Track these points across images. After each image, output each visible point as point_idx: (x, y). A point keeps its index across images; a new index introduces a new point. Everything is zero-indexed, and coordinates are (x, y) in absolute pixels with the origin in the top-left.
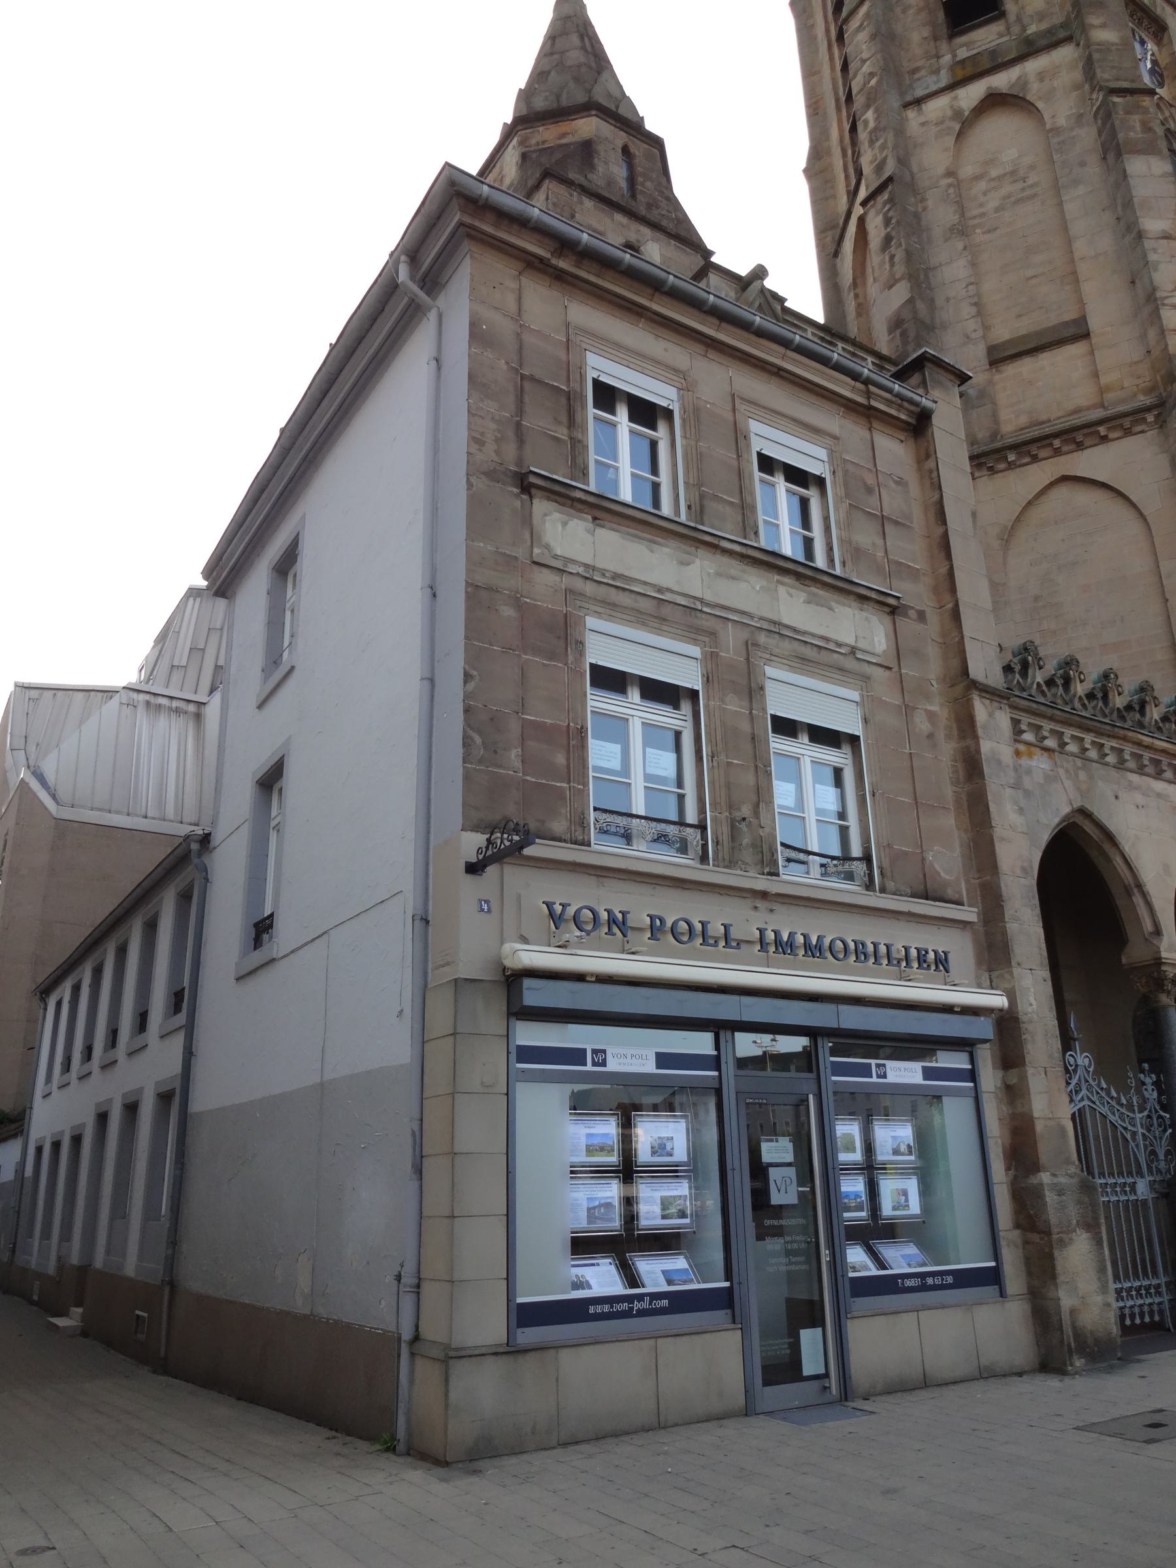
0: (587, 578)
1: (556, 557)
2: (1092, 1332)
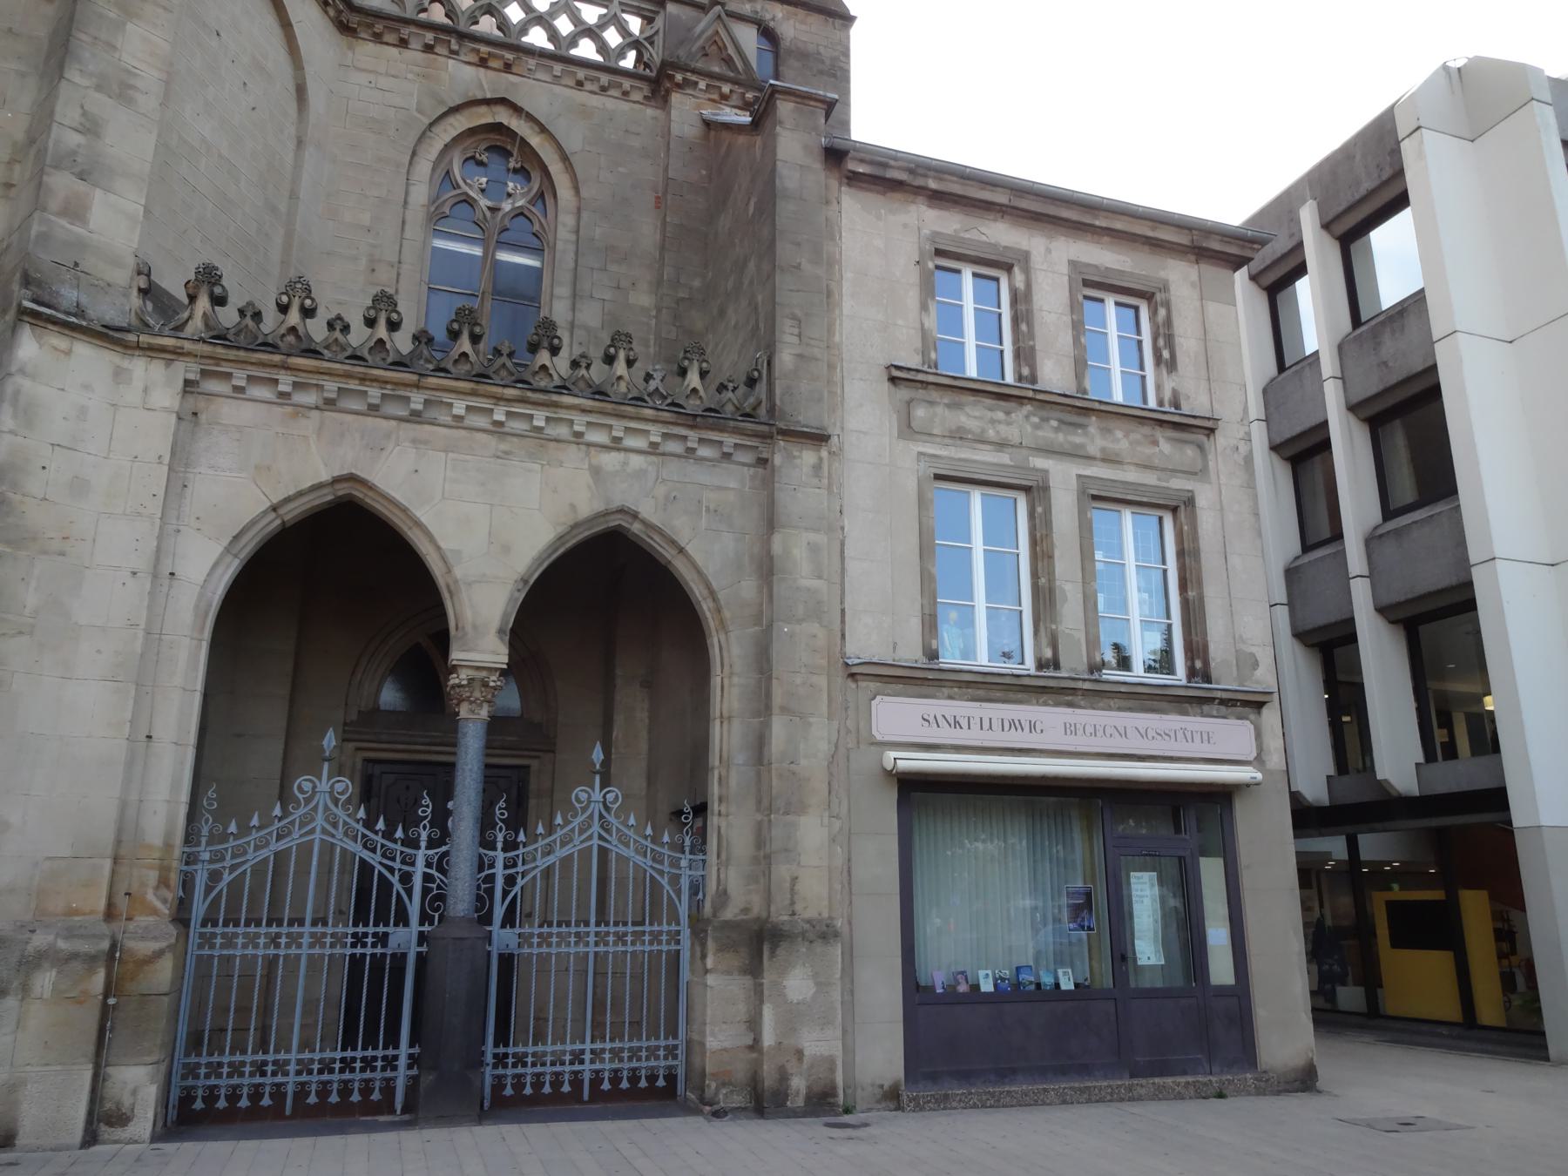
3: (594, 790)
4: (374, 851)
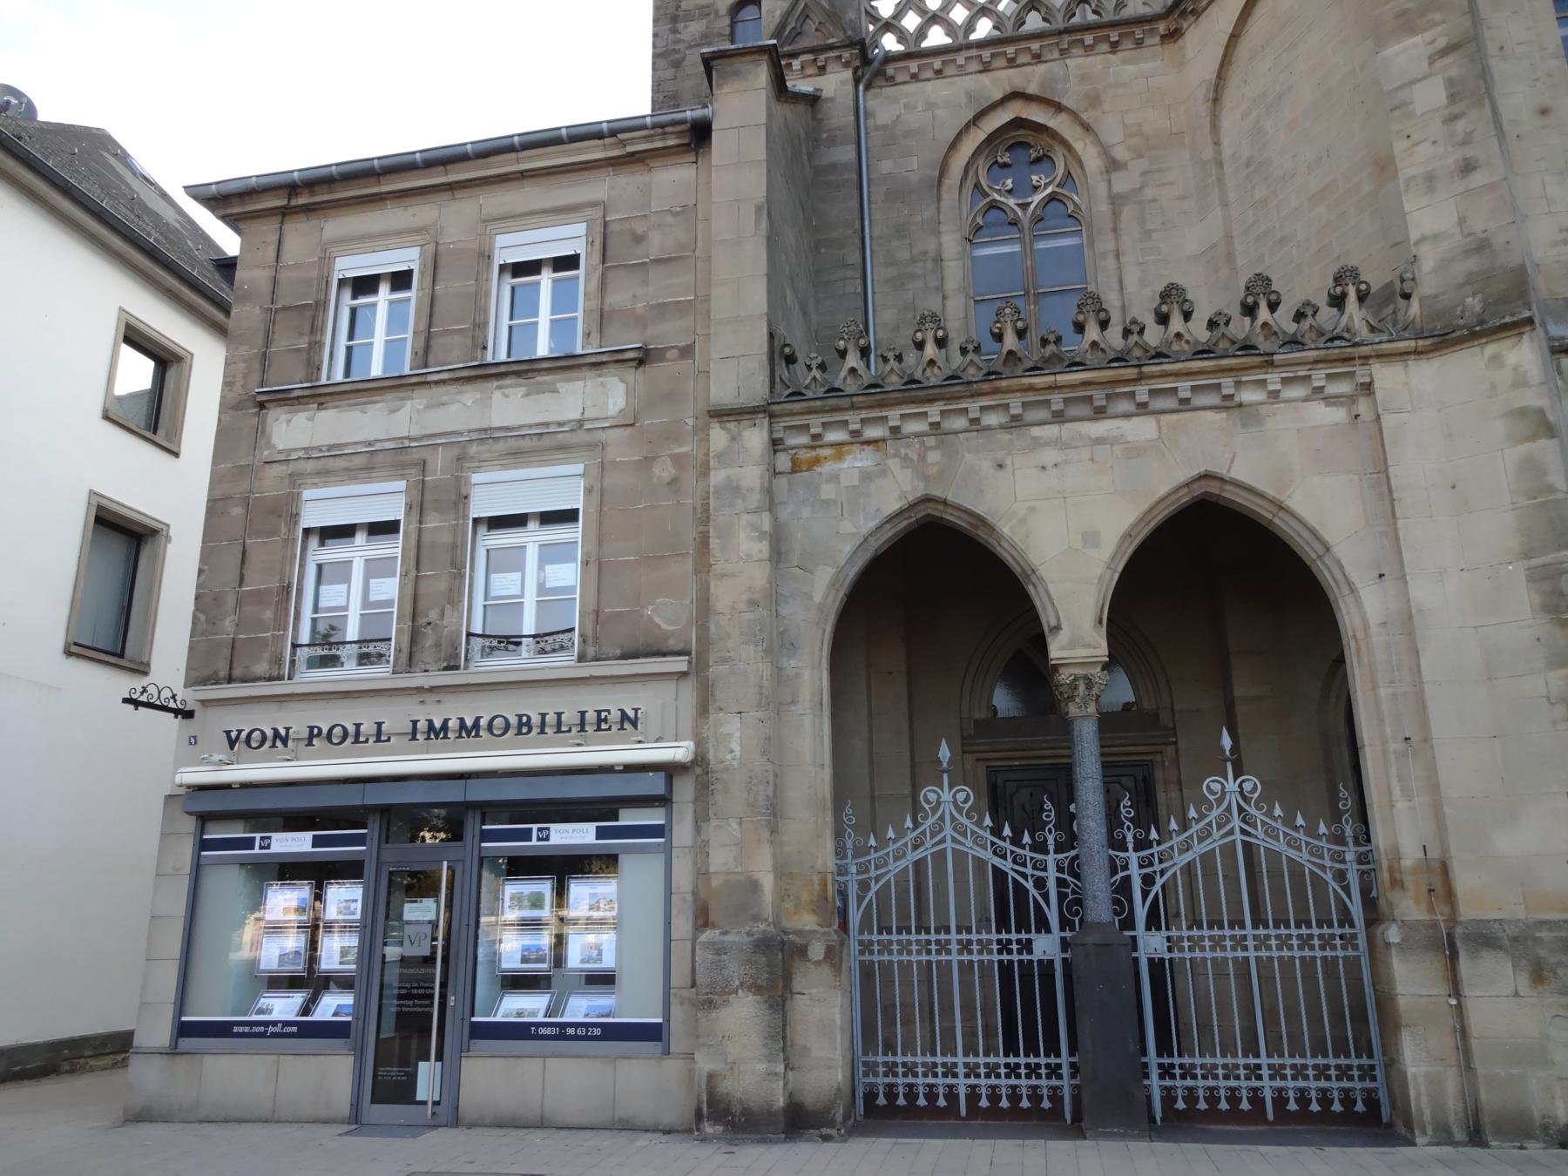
1: (280, 452)
2: (741, 1101)
3: (1227, 780)
4: (1004, 857)
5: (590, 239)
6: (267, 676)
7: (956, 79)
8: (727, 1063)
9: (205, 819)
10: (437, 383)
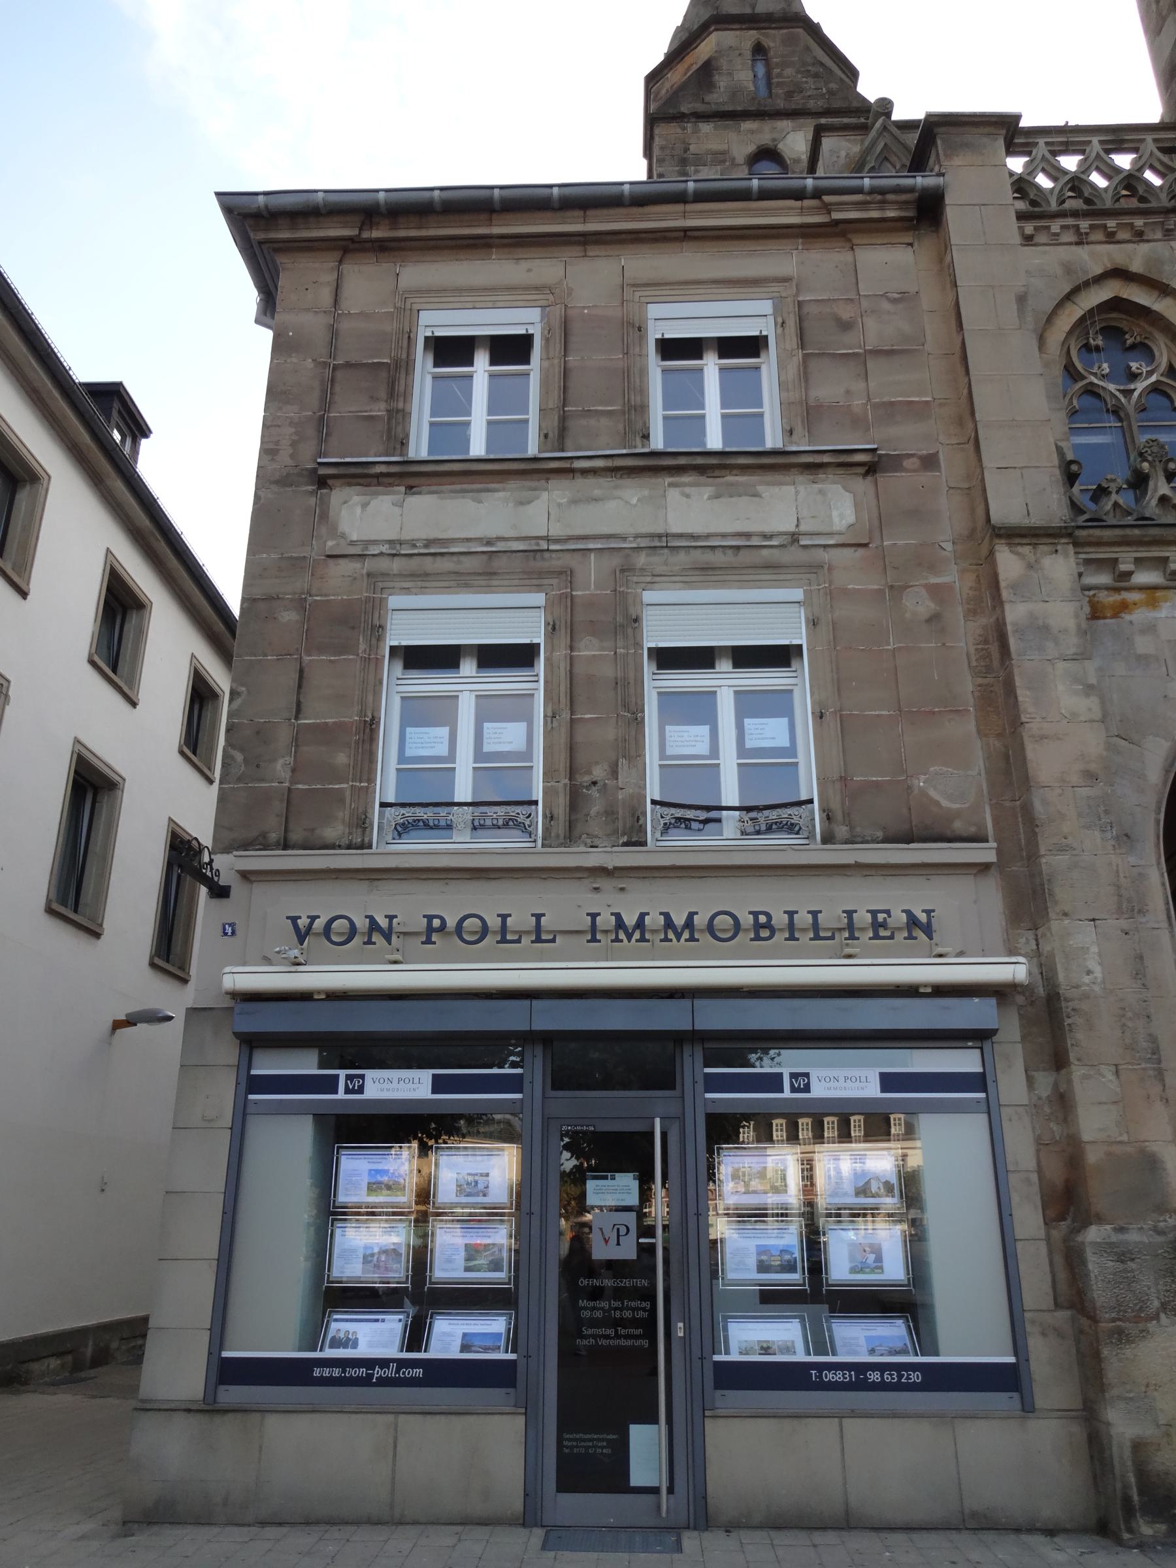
0: (394, 555)
5: (780, 320)
6: (345, 841)
7: (1047, 248)
8: (1158, 1426)
9: (252, 1043)
10: (585, 472)
